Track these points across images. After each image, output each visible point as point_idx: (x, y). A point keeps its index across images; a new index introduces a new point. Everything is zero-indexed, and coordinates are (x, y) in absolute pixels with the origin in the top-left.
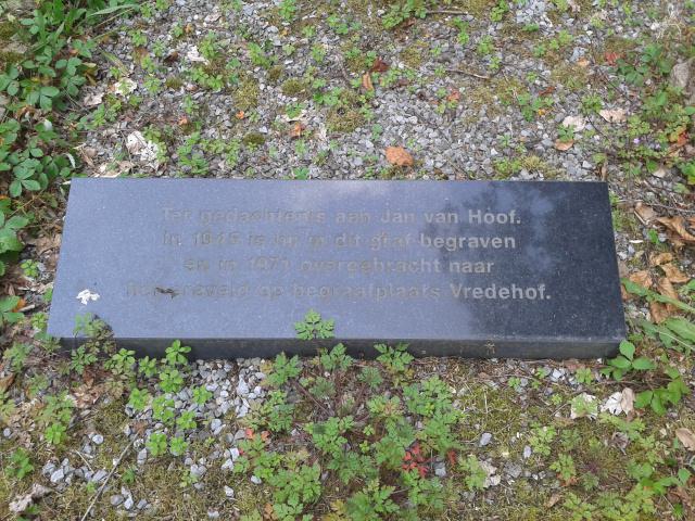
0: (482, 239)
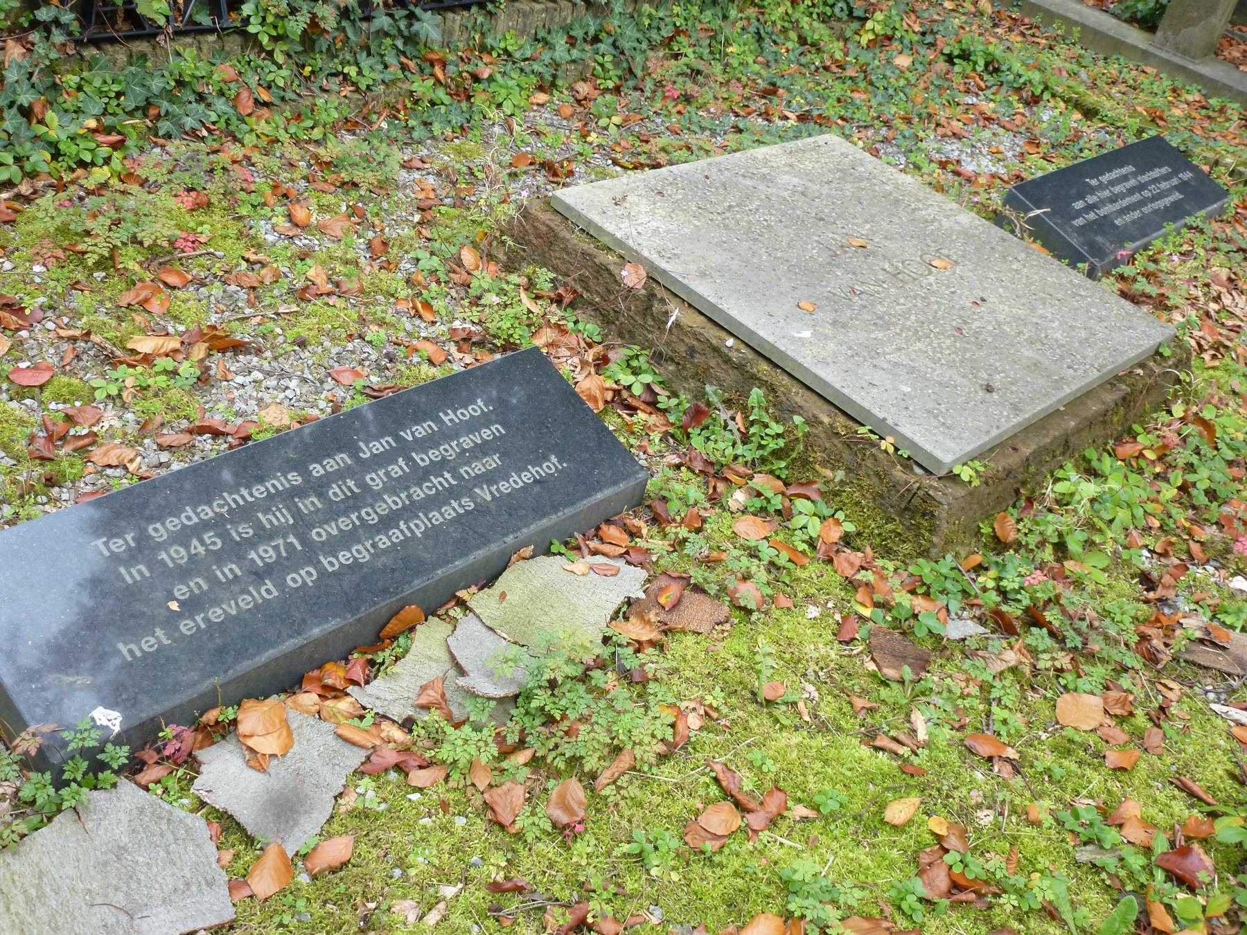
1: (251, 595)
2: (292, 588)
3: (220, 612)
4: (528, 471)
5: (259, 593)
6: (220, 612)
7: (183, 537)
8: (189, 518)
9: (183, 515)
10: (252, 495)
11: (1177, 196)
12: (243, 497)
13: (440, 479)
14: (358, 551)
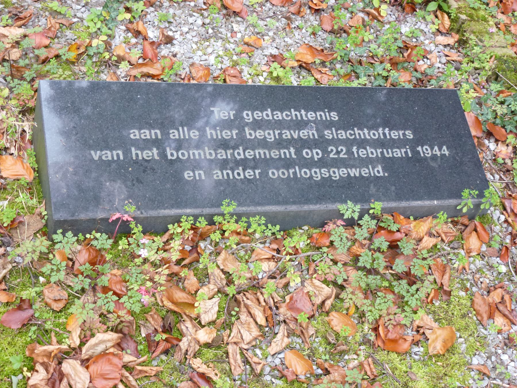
0: (292, 132)
1: (369, 169)
2: (271, 178)
3: (346, 172)
4: (365, 149)
5: (300, 172)
6: (346, 172)
7: (257, 125)
8: (267, 115)
9: (265, 113)
10: (369, 135)
11: (379, 171)
12: (301, 115)
13: (298, 113)
14: (316, 173)
